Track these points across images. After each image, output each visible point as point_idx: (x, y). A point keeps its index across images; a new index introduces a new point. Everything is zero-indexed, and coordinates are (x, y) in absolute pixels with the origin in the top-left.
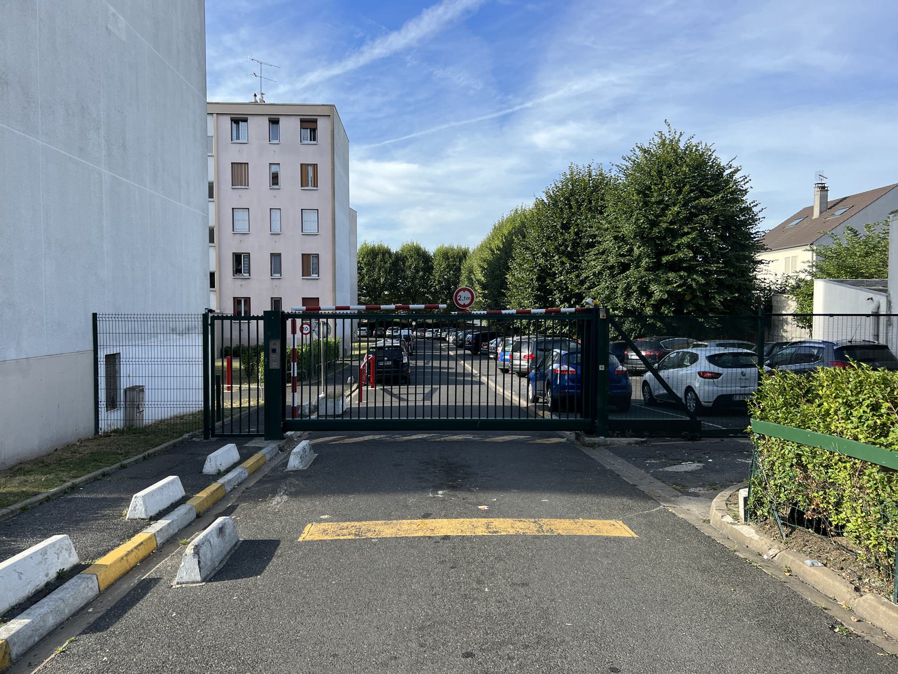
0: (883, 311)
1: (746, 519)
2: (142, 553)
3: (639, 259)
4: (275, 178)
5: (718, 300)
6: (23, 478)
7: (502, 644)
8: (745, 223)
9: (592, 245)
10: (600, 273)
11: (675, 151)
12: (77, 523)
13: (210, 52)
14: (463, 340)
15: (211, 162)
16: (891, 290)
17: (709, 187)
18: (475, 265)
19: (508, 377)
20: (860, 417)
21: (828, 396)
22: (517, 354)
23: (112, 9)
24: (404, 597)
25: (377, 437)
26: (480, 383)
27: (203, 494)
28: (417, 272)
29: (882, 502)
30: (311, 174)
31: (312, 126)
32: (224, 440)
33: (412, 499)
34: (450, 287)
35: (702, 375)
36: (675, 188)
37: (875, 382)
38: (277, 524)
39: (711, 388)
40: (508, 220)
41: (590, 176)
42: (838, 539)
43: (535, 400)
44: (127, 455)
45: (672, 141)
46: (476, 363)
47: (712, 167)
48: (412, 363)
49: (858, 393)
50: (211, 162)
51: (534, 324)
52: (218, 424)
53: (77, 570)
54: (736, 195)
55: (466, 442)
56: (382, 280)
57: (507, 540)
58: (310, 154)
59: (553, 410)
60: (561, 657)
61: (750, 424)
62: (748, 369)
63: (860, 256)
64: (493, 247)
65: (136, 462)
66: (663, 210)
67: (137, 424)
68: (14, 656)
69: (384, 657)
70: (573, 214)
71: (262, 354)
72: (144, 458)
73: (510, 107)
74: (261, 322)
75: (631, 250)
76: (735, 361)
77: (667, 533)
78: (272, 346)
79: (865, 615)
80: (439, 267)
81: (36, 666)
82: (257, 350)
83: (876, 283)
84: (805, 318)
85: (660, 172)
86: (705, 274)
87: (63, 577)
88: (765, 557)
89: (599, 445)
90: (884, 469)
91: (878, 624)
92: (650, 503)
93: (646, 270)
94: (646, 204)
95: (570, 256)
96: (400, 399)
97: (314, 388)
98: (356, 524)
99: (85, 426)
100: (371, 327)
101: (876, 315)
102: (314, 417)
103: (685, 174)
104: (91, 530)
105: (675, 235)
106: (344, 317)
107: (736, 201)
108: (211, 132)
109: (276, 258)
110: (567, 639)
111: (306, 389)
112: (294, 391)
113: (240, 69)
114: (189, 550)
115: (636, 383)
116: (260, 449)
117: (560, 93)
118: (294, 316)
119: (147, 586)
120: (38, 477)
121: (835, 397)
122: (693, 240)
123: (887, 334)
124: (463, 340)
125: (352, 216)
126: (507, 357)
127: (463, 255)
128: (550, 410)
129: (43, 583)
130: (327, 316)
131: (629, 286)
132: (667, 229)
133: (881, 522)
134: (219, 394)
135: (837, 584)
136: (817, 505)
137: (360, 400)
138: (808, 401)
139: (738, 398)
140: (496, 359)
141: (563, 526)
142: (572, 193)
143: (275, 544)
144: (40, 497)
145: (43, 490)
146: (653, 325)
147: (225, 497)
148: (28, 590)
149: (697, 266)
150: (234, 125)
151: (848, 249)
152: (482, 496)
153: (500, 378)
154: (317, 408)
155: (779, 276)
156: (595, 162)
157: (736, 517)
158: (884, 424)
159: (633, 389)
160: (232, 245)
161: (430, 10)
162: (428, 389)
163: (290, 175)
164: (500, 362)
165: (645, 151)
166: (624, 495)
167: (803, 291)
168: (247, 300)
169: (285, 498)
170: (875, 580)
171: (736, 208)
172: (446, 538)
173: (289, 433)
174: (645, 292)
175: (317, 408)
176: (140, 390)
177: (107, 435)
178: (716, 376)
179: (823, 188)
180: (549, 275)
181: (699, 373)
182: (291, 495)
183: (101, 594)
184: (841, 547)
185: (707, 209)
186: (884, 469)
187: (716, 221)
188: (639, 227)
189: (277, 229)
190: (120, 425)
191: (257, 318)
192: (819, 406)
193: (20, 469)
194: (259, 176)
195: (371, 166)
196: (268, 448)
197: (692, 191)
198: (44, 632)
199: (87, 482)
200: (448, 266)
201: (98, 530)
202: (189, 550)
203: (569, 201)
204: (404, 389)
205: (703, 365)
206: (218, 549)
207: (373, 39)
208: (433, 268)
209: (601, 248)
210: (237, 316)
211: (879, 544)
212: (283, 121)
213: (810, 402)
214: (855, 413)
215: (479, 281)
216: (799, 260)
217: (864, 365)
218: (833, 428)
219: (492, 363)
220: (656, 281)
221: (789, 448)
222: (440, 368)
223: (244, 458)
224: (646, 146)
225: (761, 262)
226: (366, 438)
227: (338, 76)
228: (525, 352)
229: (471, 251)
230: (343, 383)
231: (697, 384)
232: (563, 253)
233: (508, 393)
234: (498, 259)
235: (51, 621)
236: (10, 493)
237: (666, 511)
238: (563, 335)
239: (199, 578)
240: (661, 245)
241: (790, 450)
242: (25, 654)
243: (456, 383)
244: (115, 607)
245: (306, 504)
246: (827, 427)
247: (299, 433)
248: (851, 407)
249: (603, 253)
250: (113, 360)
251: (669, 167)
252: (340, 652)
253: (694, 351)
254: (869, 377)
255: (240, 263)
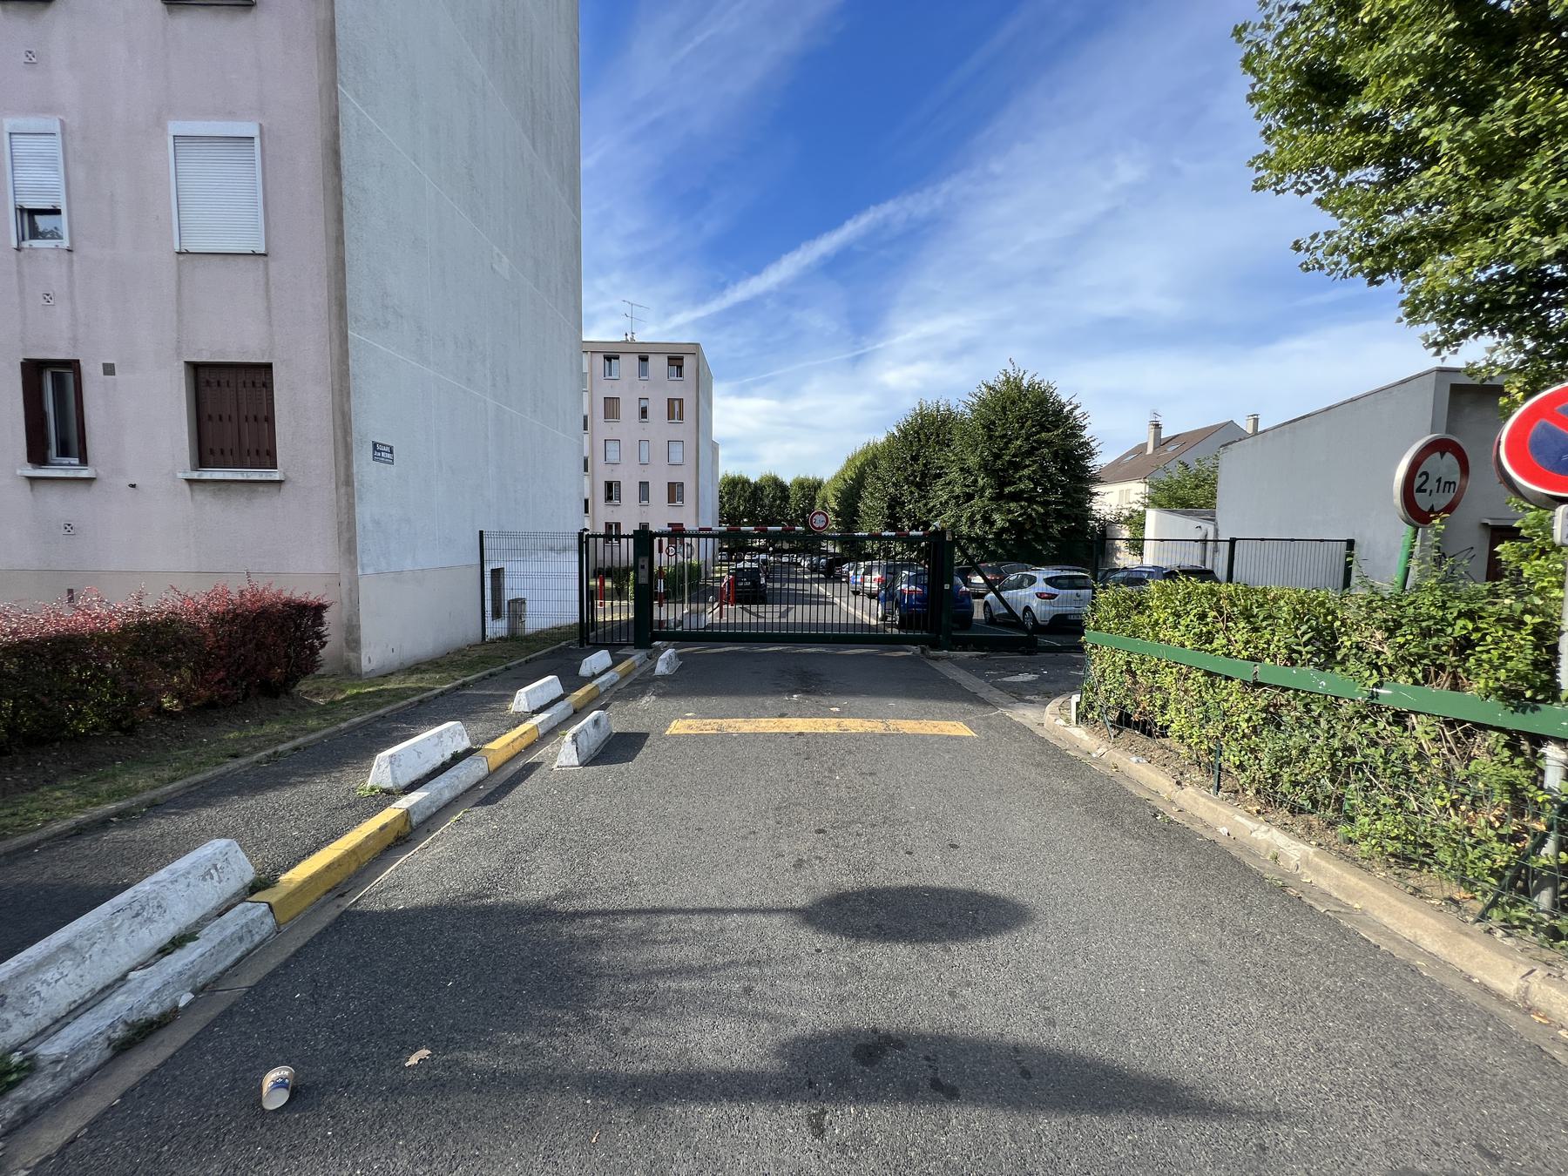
0: (1211, 537)
1: (1077, 722)
2: (525, 741)
3: (983, 489)
4: (644, 413)
5: (1056, 529)
6: (419, 676)
7: (853, 822)
8: (1083, 457)
9: (939, 476)
10: (946, 502)
11: (1019, 388)
12: (468, 714)
13: (585, 296)
14: (818, 565)
15: (586, 396)
16: (1218, 517)
17: (1051, 422)
18: (829, 494)
19: (859, 599)
20: (1188, 626)
21: (1158, 607)
22: (867, 577)
23: (496, 249)
24: (762, 783)
25: (736, 648)
26: (833, 604)
27: (580, 693)
28: (775, 500)
29: (1204, 704)
30: (677, 409)
31: (678, 363)
32: (597, 647)
33: (769, 702)
34: (805, 514)
35: (1040, 595)
36: (1018, 423)
37: (1203, 593)
38: (646, 720)
39: (1048, 608)
40: (860, 453)
41: (938, 411)
42: (1162, 740)
43: (884, 618)
44: (511, 658)
45: (1015, 379)
46: (830, 586)
47: (1053, 403)
48: (770, 585)
49: (1187, 603)
50: (586, 396)
51: (884, 550)
52: (592, 634)
53: (468, 753)
54: (1074, 430)
55: (820, 654)
56: (741, 508)
57: (856, 737)
58: (677, 389)
59: (900, 627)
60: (905, 834)
61: (1084, 635)
62: (1083, 591)
63: (1190, 488)
64: (846, 477)
65: (520, 665)
66: (1006, 443)
67: (520, 632)
68: (414, 824)
69: (744, 831)
70: (922, 447)
71: (632, 574)
72: (526, 662)
73: (863, 348)
74: (631, 540)
75: (975, 481)
76: (1072, 583)
77: (1004, 733)
78: (641, 563)
79: (1185, 806)
80: (795, 495)
81: (434, 832)
82: (627, 570)
83: (1207, 513)
84: (1137, 545)
85: (1004, 408)
86: (1045, 504)
87: (457, 758)
88: (1094, 755)
89: (943, 658)
90: (1208, 674)
91: (1197, 814)
92: (989, 708)
93: (989, 500)
94: (990, 437)
95: (918, 486)
96: (758, 617)
97: (679, 606)
98: (719, 721)
99: (473, 634)
100: (730, 552)
101: (1205, 541)
102: (679, 629)
103: (1028, 410)
104: (480, 720)
105: (1017, 467)
106: (707, 536)
107: (1076, 436)
108: (586, 369)
109: (644, 486)
110: (911, 820)
111: (672, 606)
112: (660, 606)
113: (612, 312)
114: (568, 738)
115: (978, 604)
116: (631, 656)
117: (909, 336)
118: (661, 535)
119: (530, 768)
120: (433, 675)
121: (1165, 608)
122: (1034, 472)
123: (1213, 559)
124: (818, 565)
125: (715, 447)
126: (859, 580)
127: (817, 486)
128: (897, 627)
129: (440, 763)
130: (691, 536)
131: (973, 515)
132: (1010, 462)
133: (1203, 722)
134: (592, 609)
135: (1160, 778)
136: (1144, 708)
137: (721, 617)
138: (1139, 612)
139: (1072, 618)
140: (848, 582)
141: (909, 726)
142: (922, 427)
143: (645, 736)
144: (436, 692)
145: (437, 686)
146: (994, 552)
147: (599, 696)
148: (427, 768)
149: (1037, 496)
150: (607, 362)
151: (1179, 482)
152: (834, 700)
153: (852, 599)
154: (681, 622)
155: (1114, 507)
156: (943, 398)
157: (1068, 721)
158: (1209, 632)
159: (975, 610)
160: (603, 474)
161: (788, 256)
162: (784, 608)
163: (658, 409)
164: (852, 585)
165: (990, 388)
166: (964, 701)
167: (1137, 521)
168: (618, 525)
169: (654, 697)
170: (1196, 775)
171: (1075, 442)
172: (800, 734)
173: (656, 643)
174: (987, 520)
175: (681, 622)
176: (522, 601)
177: (493, 641)
178: (1053, 596)
179: (1157, 426)
180: (899, 503)
181: (1037, 594)
182: (659, 695)
183: (490, 774)
184: (1163, 747)
185: (1048, 444)
186: (1208, 674)
187: (1056, 455)
188: (983, 459)
189: (645, 459)
190: (504, 633)
191: (628, 537)
192: (1149, 616)
193: (418, 669)
194: (629, 410)
195: (734, 403)
196: (637, 656)
197: (1034, 426)
198: (441, 803)
199: (476, 680)
200: (804, 495)
201: (486, 721)
202: (568, 738)
203: (919, 434)
204: (761, 608)
205: (1041, 586)
206: (592, 740)
207: (735, 283)
208: (789, 497)
209: (948, 479)
210: (608, 537)
211: (1201, 742)
212: (651, 358)
213: (1142, 613)
214: (1182, 622)
215: (833, 509)
216: (1132, 492)
217: (1193, 579)
218: (1161, 636)
219: (845, 586)
220: (998, 510)
221: (1120, 655)
222: (796, 590)
223: (615, 663)
224: (991, 383)
225: (1096, 494)
226: (727, 649)
227: (702, 318)
228: (876, 575)
229: (825, 482)
230: (706, 601)
231: (1035, 604)
232: (912, 483)
233: (859, 613)
234: (851, 488)
235: (447, 795)
236: (409, 688)
237: (1003, 715)
238: (910, 560)
239: (577, 763)
240: (1004, 477)
241: (1120, 658)
242: (424, 822)
243: (810, 603)
244: (502, 785)
245: (672, 704)
246: (1156, 635)
247: (665, 643)
248: (1179, 616)
249: (949, 483)
250: (497, 574)
251: (1013, 403)
252: (704, 827)
253: (1033, 574)
254: (1197, 588)
255: (611, 491)
